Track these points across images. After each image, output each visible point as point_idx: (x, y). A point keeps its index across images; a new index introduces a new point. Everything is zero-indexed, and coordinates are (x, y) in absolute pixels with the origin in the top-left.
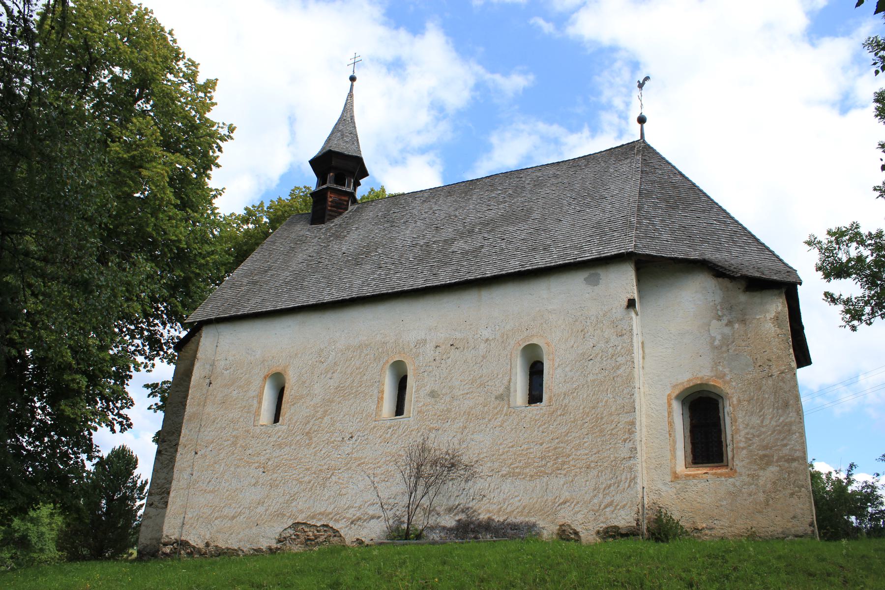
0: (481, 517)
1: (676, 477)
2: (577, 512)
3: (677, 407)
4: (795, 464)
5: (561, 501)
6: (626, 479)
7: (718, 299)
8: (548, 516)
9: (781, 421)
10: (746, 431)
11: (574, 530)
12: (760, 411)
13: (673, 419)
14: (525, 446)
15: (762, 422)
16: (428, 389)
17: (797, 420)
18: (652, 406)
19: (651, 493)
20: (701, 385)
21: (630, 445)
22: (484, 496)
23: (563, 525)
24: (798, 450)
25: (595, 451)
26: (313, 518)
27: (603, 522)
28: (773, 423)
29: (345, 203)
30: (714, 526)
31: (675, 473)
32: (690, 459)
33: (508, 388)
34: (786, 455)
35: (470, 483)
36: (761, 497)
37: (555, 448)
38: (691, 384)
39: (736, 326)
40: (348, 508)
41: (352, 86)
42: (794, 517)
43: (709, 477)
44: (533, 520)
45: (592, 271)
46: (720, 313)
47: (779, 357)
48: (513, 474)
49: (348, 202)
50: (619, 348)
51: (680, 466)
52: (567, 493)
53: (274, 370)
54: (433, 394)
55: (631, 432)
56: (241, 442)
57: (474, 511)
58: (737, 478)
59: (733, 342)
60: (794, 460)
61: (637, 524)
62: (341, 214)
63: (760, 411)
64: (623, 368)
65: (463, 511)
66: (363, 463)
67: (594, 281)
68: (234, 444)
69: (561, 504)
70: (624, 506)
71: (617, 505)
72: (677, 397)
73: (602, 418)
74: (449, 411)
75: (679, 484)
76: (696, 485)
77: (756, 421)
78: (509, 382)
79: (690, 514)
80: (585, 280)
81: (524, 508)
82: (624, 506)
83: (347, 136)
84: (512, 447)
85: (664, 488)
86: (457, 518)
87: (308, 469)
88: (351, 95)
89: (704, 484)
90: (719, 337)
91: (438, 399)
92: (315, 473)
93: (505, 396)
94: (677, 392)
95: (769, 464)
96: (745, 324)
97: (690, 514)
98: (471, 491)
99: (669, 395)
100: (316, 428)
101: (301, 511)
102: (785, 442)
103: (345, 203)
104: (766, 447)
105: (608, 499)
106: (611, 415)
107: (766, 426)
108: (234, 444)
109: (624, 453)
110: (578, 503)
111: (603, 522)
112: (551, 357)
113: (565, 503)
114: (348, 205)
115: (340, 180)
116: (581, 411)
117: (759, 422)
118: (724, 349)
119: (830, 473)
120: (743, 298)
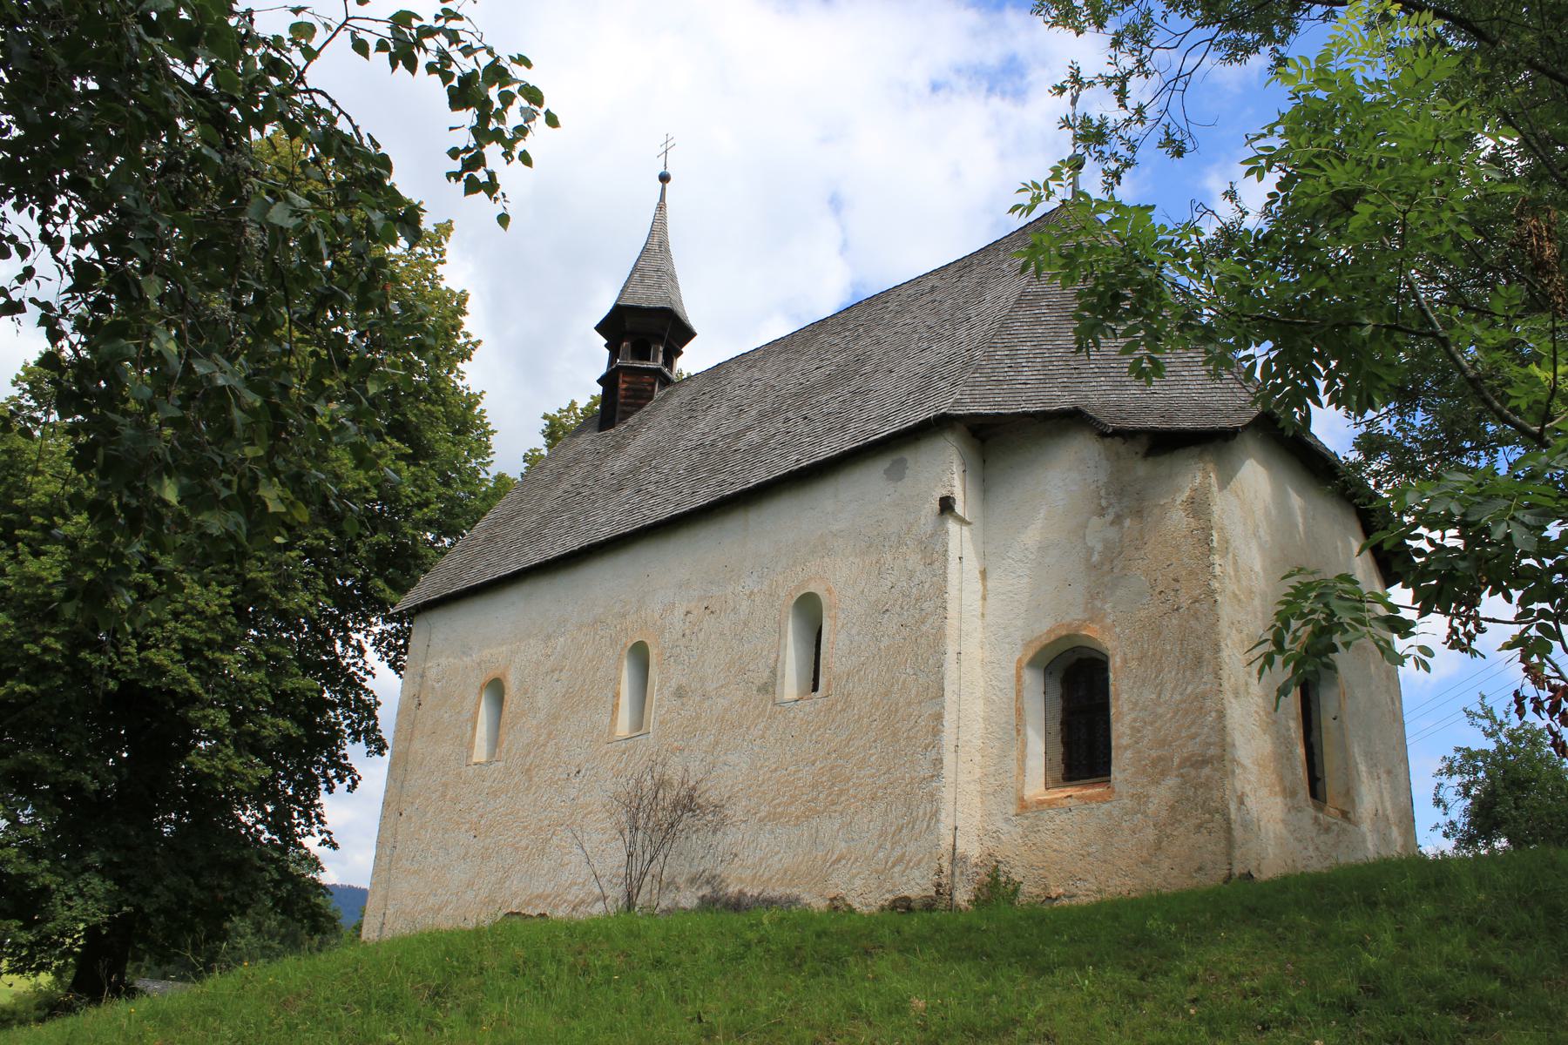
0: (730, 890)
1: (1023, 806)
2: (854, 877)
3: (1034, 683)
4: (1207, 771)
5: (834, 858)
6: (925, 814)
7: (1103, 478)
8: (815, 884)
9: (1189, 691)
10: (1133, 715)
11: (849, 906)
12: (1156, 677)
13: (1022, 703)
14: (792, 768)
15: (1159, 696)
16: (674, 684)
17: (1215, 687)
18: (994, 683)
19: (986, 838)
20: (1068, 637)
21: (932, 755)
22: (736, 855)
23: (835, 898)
24: (1213, 744)
25: (884, 769)
26: (528, 904)
27: (889, 891)
28: (1177, 697)
29: (649, 388)
30: (1075, 891)
31: (1022, 799)
32: (1059, 772)
33: (774, 672)
34: (1193, 755)
35: (719, 834)
36: (1150, 834)
37: (832, 769)
38: (1053, 638)
39: (1127, 522)
40: (570, 886)
41: (663, 189)
42: (1200, 869)
43: (1072, 802)
44: (796, 891)
45: (895, 456)
46: (1104, 503)
47: (1191, 573)
48: (773, 817)
49: (653, 385)
50: (927, 585)
51: (1035, 784)
52: (843, 844)
53: (492, 675)
54: (680, 693)
55: (936, 732)
56: (450, 793)
57: (722, 881)
58: (1114, 803)
59: (1120, 553)
60: (1205, 762)
61: (937, 892)
62: (641, 407)
63: (1156, 677)
64: (930, 621)
65: (708, 882)
66: (590, 813)
67: (896, 474)
68: (443, 795)
69: (834, 863)
70: (920, 862)
71: (910, 861)
72: (1033, 663)
73: (897, 711)
74: (698, 718)
75: (1027, 818)
76: (1052, 819)
77: (1149, 695)
78: (776, 661)
79: (1041, 871)
80: (886, 472)
81: (785, 873)
82: (920, 862)
83: (652, 277)
84: (776, 770)
85: (1006, 827)
86: (700, 894)
87: (525, 828)
88: (661, 206)
89: (1065, 816)
90: (1099, 547)
91: (685, 700)
92: (533, 833)
93: (769, 687)
94: (1031, 654)
95: (1163, 774)
96: (1141, 517)
97: (1041, 871)
98: (720, 848)
99: (1020, 660)
100: (537, 761)
101: (515, 895)
102: (1193, 730)
103: (649, 388)
104: (1162, 743)
105: (897, 853)
106: (909, 704)
107: (1165, 702)
108: (443, 795)
109: (925, 771)
110: (856, 860)
111: (889, 891)
112: (833, 613)
113: (838, 860)
114: (653, 390)
115: (642, 352)
116: (869, 701)
117: (1154, 696)
118: (1106, 568)
119: (353, 742)
120: (1142, 469)
